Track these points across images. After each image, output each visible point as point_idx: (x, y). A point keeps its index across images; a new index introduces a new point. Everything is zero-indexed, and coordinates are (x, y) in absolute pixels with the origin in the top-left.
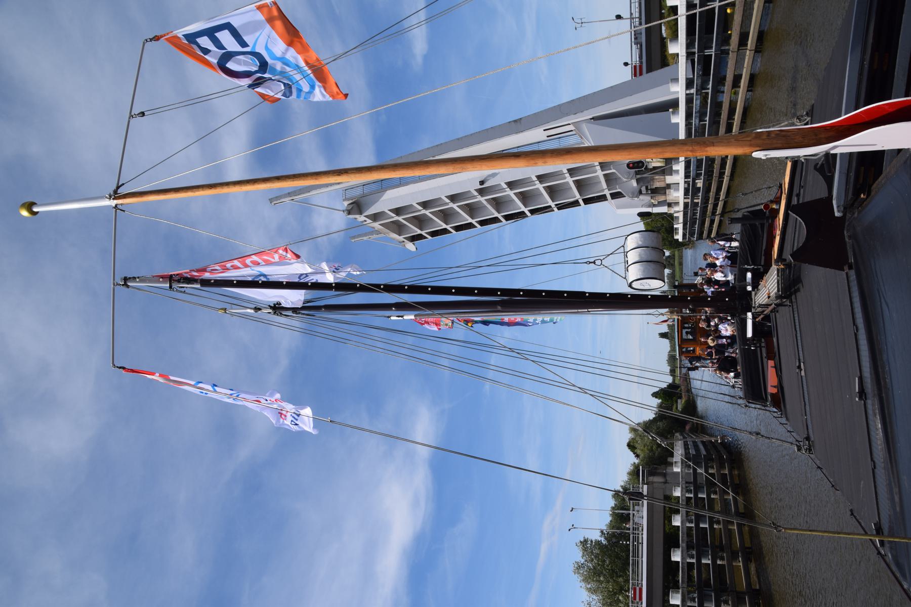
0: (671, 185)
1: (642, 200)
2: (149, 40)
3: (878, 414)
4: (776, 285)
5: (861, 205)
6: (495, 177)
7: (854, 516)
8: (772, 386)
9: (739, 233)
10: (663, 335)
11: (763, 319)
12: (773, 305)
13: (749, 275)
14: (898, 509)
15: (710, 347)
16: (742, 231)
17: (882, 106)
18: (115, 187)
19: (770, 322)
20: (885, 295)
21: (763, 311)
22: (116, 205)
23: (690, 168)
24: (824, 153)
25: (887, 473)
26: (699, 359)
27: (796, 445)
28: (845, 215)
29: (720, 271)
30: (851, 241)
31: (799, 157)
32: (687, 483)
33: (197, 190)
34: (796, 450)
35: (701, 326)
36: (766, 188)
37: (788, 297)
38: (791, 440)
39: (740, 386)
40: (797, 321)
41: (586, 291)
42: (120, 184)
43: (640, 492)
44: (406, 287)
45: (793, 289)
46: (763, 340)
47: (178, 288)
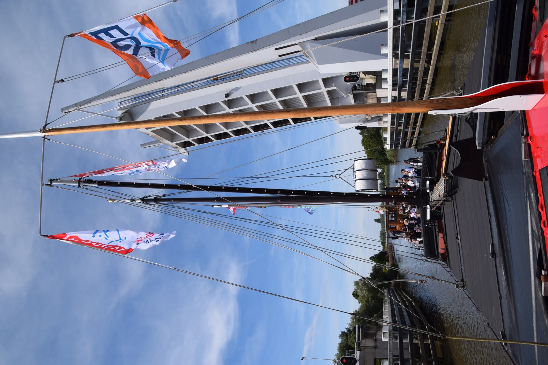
0: (381, 98)
1: (359, 117)
2: (67, 36)
3: (502, 267)
4: (444, 189)
5: (492, 142)
6: (238, 91)
7: (490, 327)
8: (441, 249)
9: (422, 158)
10: (377, 221)
11: (436, 209)
12: (442, 201)
13: (428, 183)
14: (514, 324)
15: (405, 225)
16: (424, 156)
17: (502, 86)
18: (44, 125)
19: (440, 211)
20: (506, 196)
21: (436, 204)
22: (44, 136)
23: (397, 75)
24: (470, 112)
25: (508, 302)
26: (398, 232)
27: (456, 284)
28: (483, 148)
29: (411, 180)
30: (486, 164)
31: (455, 114)
32: (394, 356)
33: (95, 128)
34: (456, 287)
35: (399, 213)
36: (438, 131)
37: (451, 196)
38: (453, 281)
39: (423, 249)
40: (456, 210)
41: (331, 192)
42: (47, 123)
43: (355, 358)
44: (223, 188)
45: (454, 191)
46: (436, 221)
47: (84, 187)
